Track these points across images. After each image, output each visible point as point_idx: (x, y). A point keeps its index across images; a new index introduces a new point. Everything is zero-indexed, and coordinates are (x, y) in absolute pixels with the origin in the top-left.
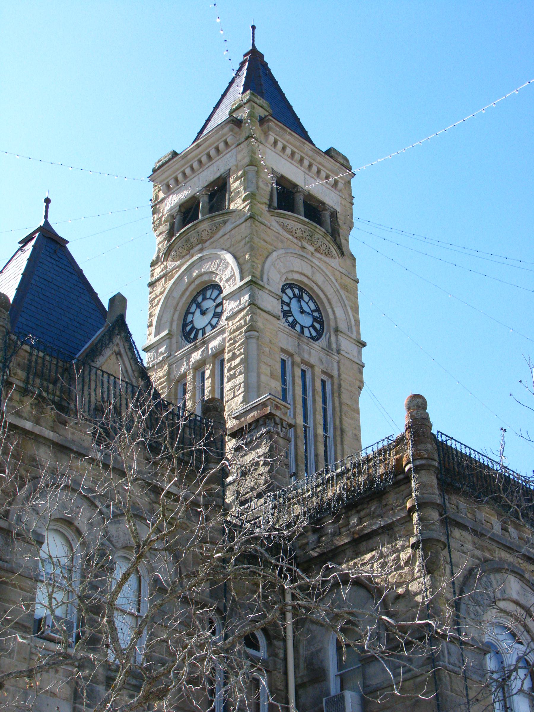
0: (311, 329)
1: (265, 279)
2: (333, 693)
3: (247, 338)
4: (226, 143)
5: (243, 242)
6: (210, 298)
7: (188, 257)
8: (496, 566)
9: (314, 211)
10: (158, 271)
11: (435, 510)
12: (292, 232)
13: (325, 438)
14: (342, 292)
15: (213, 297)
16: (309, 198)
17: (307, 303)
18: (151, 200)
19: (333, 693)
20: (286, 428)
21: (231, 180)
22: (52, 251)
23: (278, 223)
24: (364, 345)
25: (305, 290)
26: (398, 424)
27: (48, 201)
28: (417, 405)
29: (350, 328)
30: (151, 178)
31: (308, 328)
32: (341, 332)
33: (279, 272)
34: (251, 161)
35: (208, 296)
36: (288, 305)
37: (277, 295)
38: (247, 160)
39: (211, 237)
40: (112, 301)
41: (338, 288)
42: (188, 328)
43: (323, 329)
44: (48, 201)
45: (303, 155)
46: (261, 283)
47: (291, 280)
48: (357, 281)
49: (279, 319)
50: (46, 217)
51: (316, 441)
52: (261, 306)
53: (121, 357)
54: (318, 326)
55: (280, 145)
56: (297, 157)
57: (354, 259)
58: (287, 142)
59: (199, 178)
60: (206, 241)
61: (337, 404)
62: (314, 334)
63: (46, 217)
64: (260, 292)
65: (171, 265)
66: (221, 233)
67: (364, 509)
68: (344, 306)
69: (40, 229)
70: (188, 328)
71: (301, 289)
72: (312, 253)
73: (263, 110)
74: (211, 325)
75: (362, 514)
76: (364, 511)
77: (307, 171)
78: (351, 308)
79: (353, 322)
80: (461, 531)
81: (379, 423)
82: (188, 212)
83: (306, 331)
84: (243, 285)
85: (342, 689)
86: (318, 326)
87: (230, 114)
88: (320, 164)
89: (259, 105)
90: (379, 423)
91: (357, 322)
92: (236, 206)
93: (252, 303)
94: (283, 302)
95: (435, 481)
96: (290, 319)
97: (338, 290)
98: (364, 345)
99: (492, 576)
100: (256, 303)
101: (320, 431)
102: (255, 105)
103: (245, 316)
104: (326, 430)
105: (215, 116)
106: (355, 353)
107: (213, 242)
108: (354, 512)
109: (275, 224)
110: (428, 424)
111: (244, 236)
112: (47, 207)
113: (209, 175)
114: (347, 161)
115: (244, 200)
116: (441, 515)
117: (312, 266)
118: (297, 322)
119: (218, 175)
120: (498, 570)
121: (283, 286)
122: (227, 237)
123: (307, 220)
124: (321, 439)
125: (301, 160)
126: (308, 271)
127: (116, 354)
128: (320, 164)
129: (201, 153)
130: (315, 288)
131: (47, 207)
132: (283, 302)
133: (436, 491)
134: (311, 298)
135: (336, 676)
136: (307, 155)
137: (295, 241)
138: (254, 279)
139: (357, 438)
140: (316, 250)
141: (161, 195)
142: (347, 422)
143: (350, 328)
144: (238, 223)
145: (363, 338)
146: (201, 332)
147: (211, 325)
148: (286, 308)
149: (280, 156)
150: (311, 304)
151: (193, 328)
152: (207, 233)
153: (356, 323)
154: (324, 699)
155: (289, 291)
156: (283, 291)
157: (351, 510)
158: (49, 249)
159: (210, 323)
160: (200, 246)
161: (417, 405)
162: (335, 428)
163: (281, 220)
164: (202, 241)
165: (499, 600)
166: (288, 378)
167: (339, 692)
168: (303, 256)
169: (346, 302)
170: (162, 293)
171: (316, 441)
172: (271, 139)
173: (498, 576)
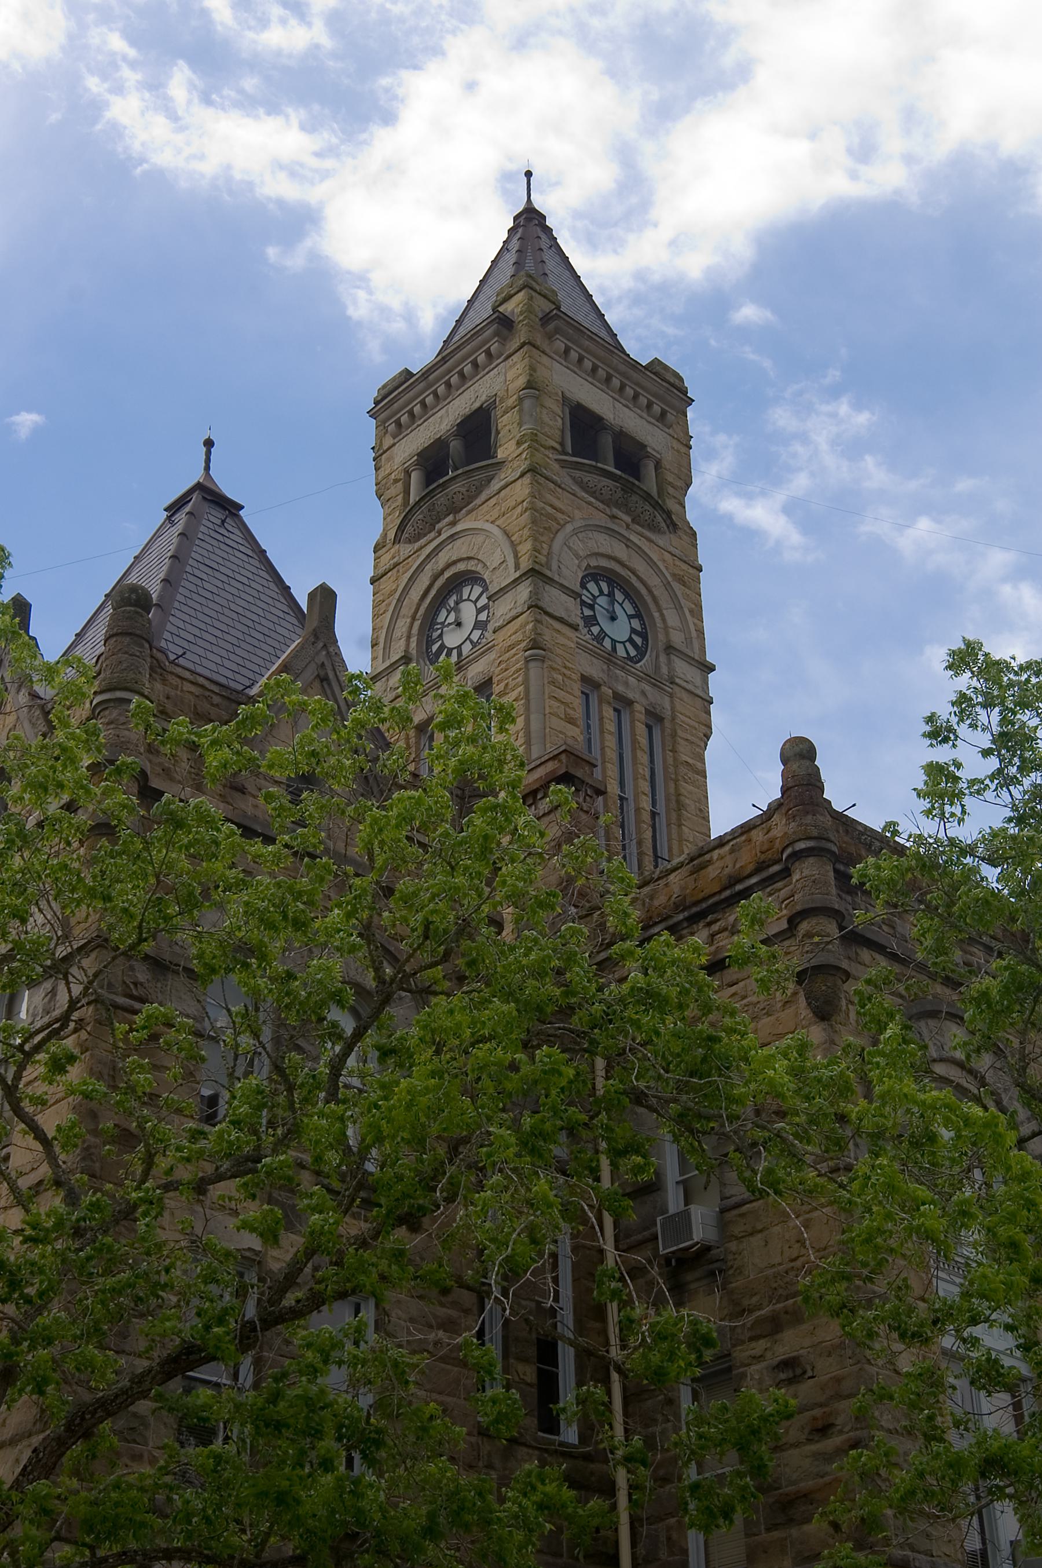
0: (627, 644)
1: (554, 567)
2: (672, 1210)
3: (527, 661)
4: (488, 353)
5: (519, 509)
6: (468, 599)
7: (433, 535)
8: (929, 1008)
9: (630, 457)
10: (386, 560)
11: (831, 920)
12: (595, 492)
13: (654, 814)
14: (676, 585)
15: (473, 597)
16: (621, 436)
17: (621, 605)
18: (373, 448)
19: (672, 1210)
20: (591, 797)
21: (499, 413)
22: (219, 522)
23: (574, 479)
24: (711, 668)
25: (618, 584)
26: (768, 786)
27: (209, 444)
28: (800, 758)
29: (689, 640)
30: (372, 414)
31: (623, 643)
32: (675, 649)
33: (577, 556)
34: (529, 381)
35: (465, 597)
36: (591, 607)
37: (573, 591)
38: (522, 381)
39: (469, 503)
40: (312, 596)
41: (670, 579)
42: (435, 648)
43: (647, 645)
44: (209, 444)
45: (611, 372)
46: (548, 573)
47: (595, 567)
48: (700, 569)
49: (576, 630)
50: (207, 468)
51: (638, 822)
52: (549, 610)
53: (329, 684)
54: (638, 640)
55: (574, 355)
56: (601, 373)
57: (694, 534)
58: (585, 351)
59: (447, 411)
60: (461, 509)
61: (670, 761)
62: (633, 652)
63: (207, 468)
64: (547, 587)
65: (406, 549)
66: (483, 496)
67: (719, 920)
68: (679, 608)
69: (199, 487)
70: (435, 648)
71: (611, 583)
72: (628, 526)
73: (546, 301)
74: (471, 642)
75: (715, 927)
76: (718, 924)
77: (617, 397)
78: (691, 611)
79: (694, 634)
80: (873, 953)
81: (738, 791)
82: (433, 463)
83: (620, 648)
84: (520, 576)
85: (686, 1205)
86: (638, 640)
87: (495, 310)
88: (638, 384)
89: (539, 294)
90: (738, 791)
91: (701, 633)
92: (507, 453)
93: (535, 606)
94: (583, 603)
95: (832, 874)
96: (595, 630)
97: (669, 583)
98: (711, 668)
99: (922, 1024)
100: (540, 604)
101: (646, 804)
102: (534, 294)
103: (523, 626)
104: (654, 803)
105: (471, 313)
106: (698, 681)
107: (472, 510)
108: (701, 924)
109: (568, 481)
110: (818, 784)
111: (519, 500)
112: (208, 454)
113: (461, 406)
114: (681, 380)
115: (519, 444)
116: (841, 928)
117: (627, 546)
118: (606, 635)
119: (477, 405)
120: (934, 1014)
121: (583, 578)
122: (493, 501)
123: (618, 472)
124: (646, 817)
125: (608, 379)
126: (620, 551)
127: (322, 681)
128: (638, 384)
129: (450, 371)
130: (634, 580)
131: (208, 454)
132: (583, 603)
133: (834, 891)
134: (627, 596)
135: (677, 1183)
136: (616, 370)
137: (602, 506)
138: (537, 567)
139: (704, 817)
140: (633, 521)
141: (388, 441)
142: (686, 788)
143: (689, 640)
144: (510, 479)
145: (709, 658)
146: (455, 652)
147: (471, 642)
148: (588, 612)
149: (575, 373)
150: (627, 605)
151: (442, 647)
152: (461, 497)
153: (698, 636)
154: (659, 1219)
155: (592, 586)
156: (583, 585)
157: (696, 922)
158: (207, 504)
159: (468, 638)
160: (450, 518)
161: (800, 758)
162: (668, 799)
163: (578, 474)
164: (454, 509)
165: (934, 1061)
166: (594, 722)
167: (682, 1207)
168: (613, 530)
169: (683, 602)
170: (391, 595)
171: (638, 822)
172: (560, 345)
173: (932, 1023)
